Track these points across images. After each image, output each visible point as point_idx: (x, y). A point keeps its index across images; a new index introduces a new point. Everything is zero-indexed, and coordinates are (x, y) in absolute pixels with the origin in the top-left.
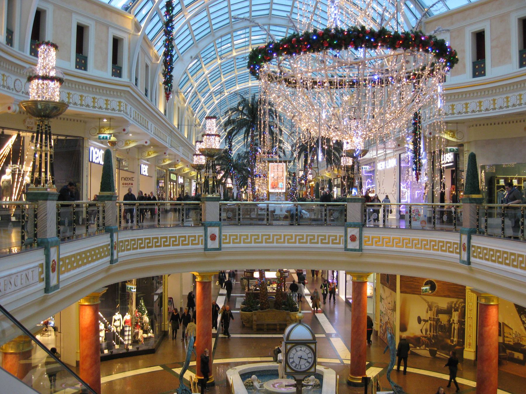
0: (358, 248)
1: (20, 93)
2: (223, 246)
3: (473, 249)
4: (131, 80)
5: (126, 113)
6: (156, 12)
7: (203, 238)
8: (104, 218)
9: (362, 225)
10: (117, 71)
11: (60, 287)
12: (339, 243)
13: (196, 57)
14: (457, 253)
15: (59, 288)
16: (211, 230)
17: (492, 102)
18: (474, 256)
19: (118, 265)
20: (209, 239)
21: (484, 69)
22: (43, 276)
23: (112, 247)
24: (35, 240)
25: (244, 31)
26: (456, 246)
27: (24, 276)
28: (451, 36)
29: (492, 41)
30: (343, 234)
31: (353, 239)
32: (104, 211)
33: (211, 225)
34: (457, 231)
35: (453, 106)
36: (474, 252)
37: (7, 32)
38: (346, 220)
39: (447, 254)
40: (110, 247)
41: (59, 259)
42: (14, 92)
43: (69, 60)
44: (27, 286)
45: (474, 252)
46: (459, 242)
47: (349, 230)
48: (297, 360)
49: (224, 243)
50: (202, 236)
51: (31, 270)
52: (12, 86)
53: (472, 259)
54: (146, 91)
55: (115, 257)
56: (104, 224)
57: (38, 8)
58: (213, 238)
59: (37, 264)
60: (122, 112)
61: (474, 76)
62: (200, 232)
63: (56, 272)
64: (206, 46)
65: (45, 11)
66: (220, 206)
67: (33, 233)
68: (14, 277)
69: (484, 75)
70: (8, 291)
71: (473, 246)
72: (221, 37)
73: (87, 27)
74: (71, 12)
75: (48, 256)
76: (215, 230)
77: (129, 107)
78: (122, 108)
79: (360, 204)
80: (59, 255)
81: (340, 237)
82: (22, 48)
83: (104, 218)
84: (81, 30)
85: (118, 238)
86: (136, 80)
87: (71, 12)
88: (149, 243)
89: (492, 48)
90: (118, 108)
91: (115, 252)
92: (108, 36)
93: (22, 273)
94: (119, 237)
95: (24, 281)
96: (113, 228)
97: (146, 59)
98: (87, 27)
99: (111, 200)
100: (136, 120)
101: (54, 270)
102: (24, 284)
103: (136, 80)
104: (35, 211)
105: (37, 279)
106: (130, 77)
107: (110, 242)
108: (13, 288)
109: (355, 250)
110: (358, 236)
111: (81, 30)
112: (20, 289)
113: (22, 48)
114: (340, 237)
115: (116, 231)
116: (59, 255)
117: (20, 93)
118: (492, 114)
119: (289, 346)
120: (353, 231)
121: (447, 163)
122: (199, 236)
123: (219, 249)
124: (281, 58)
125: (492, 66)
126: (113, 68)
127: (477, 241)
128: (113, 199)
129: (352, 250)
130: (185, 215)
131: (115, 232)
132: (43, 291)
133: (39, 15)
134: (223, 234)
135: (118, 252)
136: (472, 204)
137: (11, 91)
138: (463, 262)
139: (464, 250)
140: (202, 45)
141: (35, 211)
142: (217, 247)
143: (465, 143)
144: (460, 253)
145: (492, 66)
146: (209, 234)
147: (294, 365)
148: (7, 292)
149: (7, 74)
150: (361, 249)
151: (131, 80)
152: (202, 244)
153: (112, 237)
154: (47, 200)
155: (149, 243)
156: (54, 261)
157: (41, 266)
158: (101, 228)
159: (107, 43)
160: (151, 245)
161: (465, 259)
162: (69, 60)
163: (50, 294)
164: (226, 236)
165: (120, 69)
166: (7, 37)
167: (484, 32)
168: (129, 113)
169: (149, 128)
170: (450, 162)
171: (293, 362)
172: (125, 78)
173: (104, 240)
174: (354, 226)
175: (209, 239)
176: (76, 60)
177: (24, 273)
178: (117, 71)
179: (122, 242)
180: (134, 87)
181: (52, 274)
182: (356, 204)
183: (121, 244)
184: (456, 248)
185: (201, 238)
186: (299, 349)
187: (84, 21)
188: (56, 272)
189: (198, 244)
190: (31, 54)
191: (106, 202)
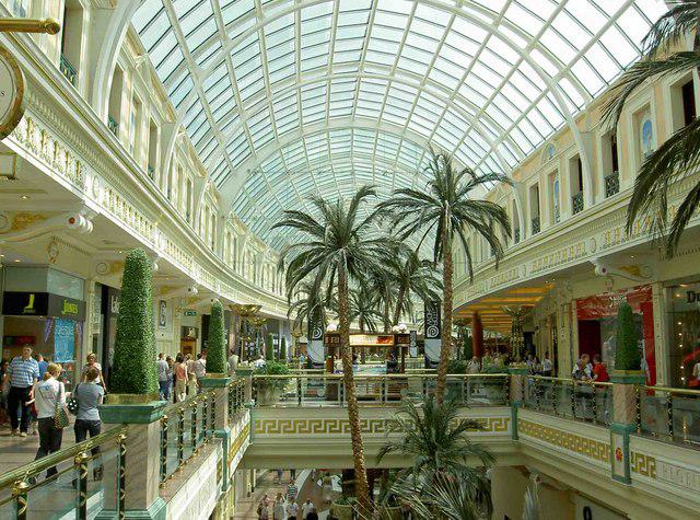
53: (633, 475)
72: (288, 145)
140: (262, 154)
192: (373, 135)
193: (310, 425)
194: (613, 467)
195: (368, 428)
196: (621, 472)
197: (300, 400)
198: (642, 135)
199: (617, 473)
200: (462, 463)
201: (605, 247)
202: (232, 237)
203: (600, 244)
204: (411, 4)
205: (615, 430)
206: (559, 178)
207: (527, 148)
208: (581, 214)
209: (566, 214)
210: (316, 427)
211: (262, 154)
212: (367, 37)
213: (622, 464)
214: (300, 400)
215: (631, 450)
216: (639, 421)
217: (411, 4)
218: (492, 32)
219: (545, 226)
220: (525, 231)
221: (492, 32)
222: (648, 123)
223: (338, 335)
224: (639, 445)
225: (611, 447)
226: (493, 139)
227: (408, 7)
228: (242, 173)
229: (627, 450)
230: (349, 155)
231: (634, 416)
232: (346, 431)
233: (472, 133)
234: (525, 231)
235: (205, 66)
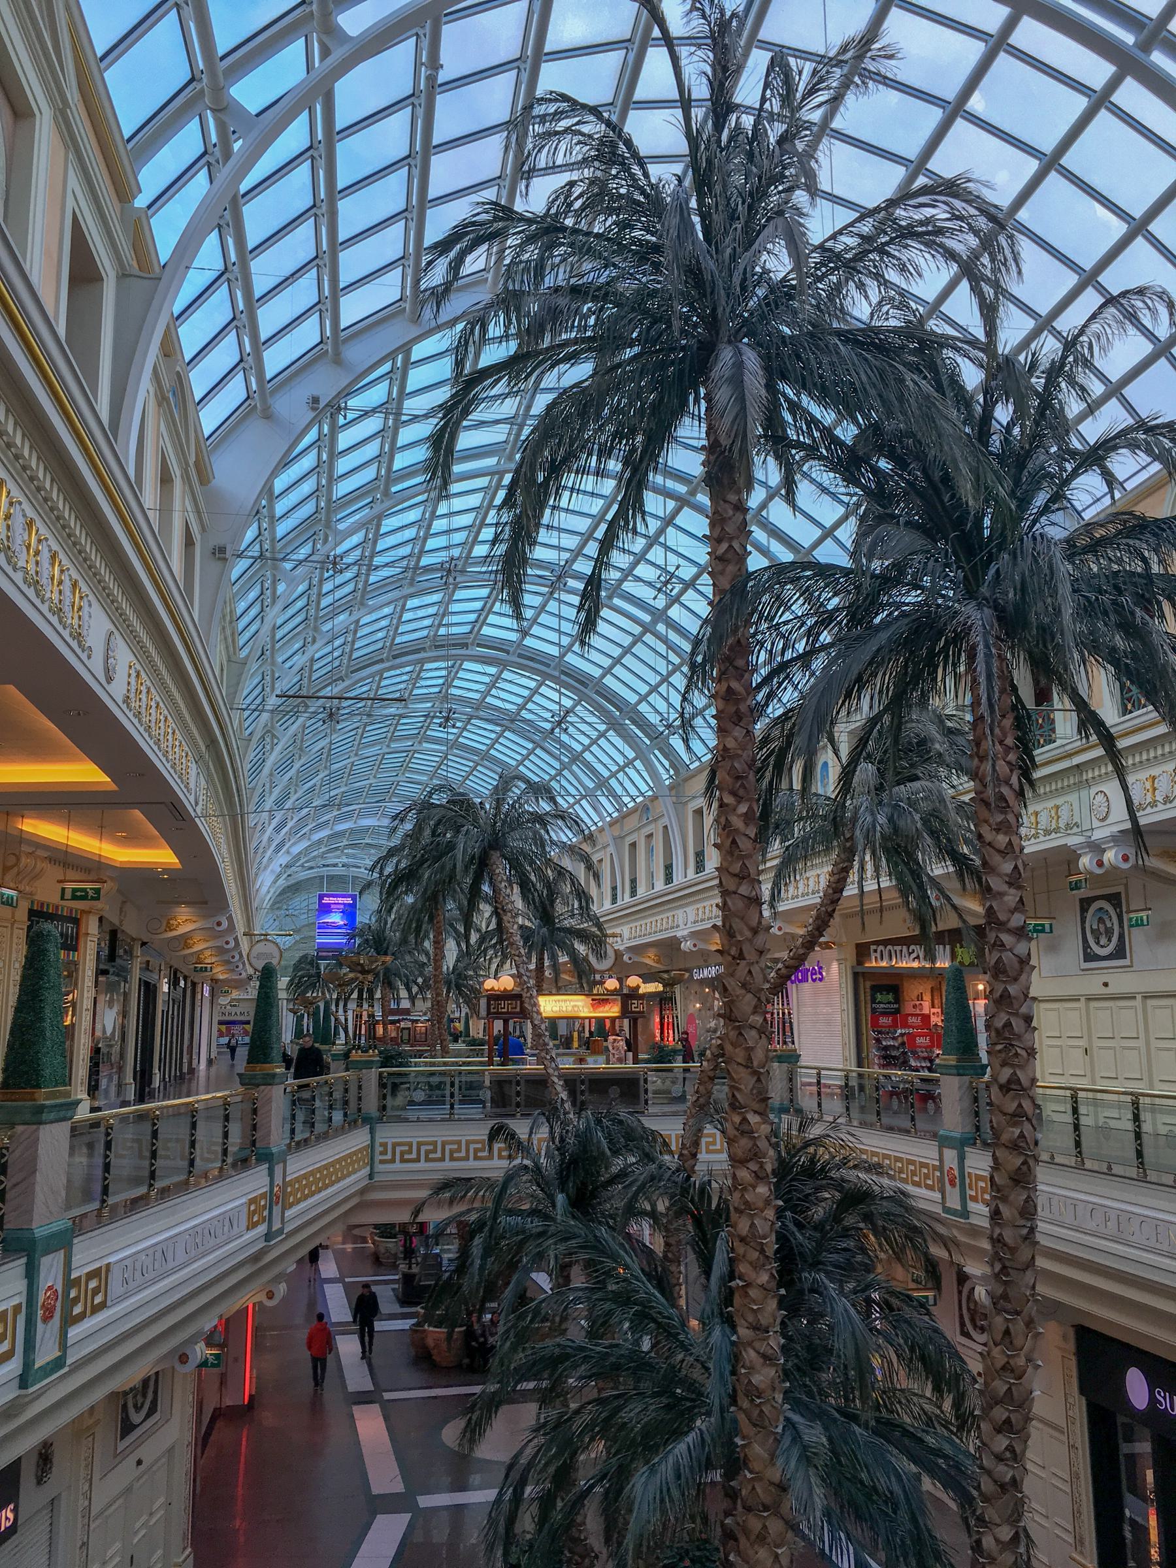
11: (69, 1362)
15: (62, 1366)
27: (159, 1255)
32: (360, 1087)
41: (69, 1283)
59: (244, 1200)
83: (360, 1099)
94: (288, 1172)
101: (46, 1319)
105: (244, 1223)
107: (21, 1299)
128: (277, 1080)
132: (16, 1382)
139: (952, 1183)
153: (31, 1273)
156: (50, 1288)
163: (31, 1390)
173: (358, 1139)
194: (943, 1197)
195: (439, 1155)
196: (954, 1203)
197: (452, 1107)
203: (691, 918)
204: (1004, 11)
205: (944, 1142)
206: (654, 842)
209: (660, 886)
210: (427, 1152)
214: (452, 1107)
215: (967, 1170)
217: (1004, 11)
218: (646, 629)
219: (641, 891)
221: (646, 629)
223: (517, 997)
225: (941, 1168)
227: (993, 17)
232: (500, 1157)
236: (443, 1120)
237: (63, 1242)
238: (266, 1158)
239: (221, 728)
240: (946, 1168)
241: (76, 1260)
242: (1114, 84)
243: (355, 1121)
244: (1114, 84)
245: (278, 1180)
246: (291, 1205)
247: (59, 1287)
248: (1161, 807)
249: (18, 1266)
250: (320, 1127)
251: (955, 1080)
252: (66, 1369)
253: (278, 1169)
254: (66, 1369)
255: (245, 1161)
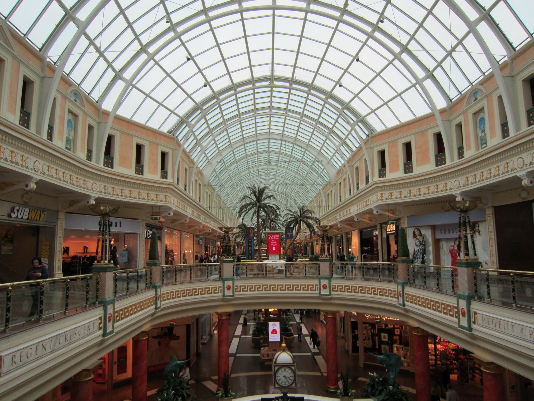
0: (328, 293)
1: (96, 192)
2: (236, 293)
3: (406, 296)
4: (174, 181)
5: (171, 203)
6: (191, 134)
7: (222, 288)
8: (151, 278)
9: (330, 278)
10: (164, 174)
11: (115, 332)
12: (315, 290)
13: (220, 162)
14: (395, 298)
15: (113, 333)
16: (227, 283)
17: (418, 190)
18: (407, 301)
19: (161, 311)
20: (226, 289)
21: (412, 168)
22: (102, 325)
23: (156, 299)
24: (97, 300)
25: (252, 144)
26: (395, 293)
27: (86, 328)
28: (389, 146)
29: (416, 149)
30: (318, 284)
31: (325, 287)
32: (151, 274)
33: (227, 279)
34: (395, 282)
35: (391, 193)
36: (407, 298)
37: (87, 151)
38: (319, 274)
39: (389, 298)
40: (154, 299)
41: (114, 312)
42: (92, 191)
43: (131, 168)
44: (88, 335)
45: (407, 298)
46: (396, 290)
47: (322, 281)
48: (283, 379)
49: (236, 291)
50: (221, 287)
51: (92, 323)
52: (90, 188)
53: (406, 303)
54: (186, 186)
55: (159, 305)
56: (151, 283)
57: (109, 134)
58: (229, 288)
59: (97, 317)
60: (168, 202)
61: (405, 173)
62: (220, 284)
63: (111, 322)
64: (227, 154)
65: (114, 136)
66: (233, 266)
67: (95, 295)
68: (78, 329)
69: (412, 172)
70: (73, 339)
71: (406, 294)
73: (144, 146)
74: (132, 136)
75: (105, 311)
76: (230, 283)
77: (172, 198)
78: (167, 200)
79: (329, 263)
80: (114, 309)
81: (316, 285)
82: (98, 162)
83: (151, 278)
84: (139, 148)
85: (161, 292)
86: (178, 179)
87: (132, 136)
88: (184, 293)
89: (416, 153)
90: (164, 200)
91: (159, 302)
92: (157, 152)
93: (84, 326)
95: (86, 331)
96: (157, 285)
97: (185, 164)
98: (144, 146)
99: (156, 266)
100: (178, 207)
101: (110, 321)
102: (86, 332)
103: (178, 179)
104: (97, 280)
105: (96, 327)
106: (173, 178)
107: (154, 295)
108: (78, 337)
109: (326, 295)
110: (328, 285)
111: (139, 148)
112: (83, 338)
113: (98, 162)
114: (316, 285)
115: (160, 287)
116: (114, 309)
117: (96, 192)
118: (418, 198)
119: (276, 368)
120: (324, 282)
121: (391, 231)
122: (219, 287)
123: (233, 296)
124: (92, 248)
125: (418, 165)
126: (161, 172)
127: (409, 290)
129: (324, 295)
130: (209, 273)
131: (159, 288)
132: (102, 336)
133: (110, 139)
134: (235, 285)
135: (161, 301)
136: (404, 264)
137: (89, 191)
138: (400, 304)
139: (400, 296)
140: (224, 154)
141: (97, 280)
142: (232, 294)
143: (402, 217)
144: (397, 298)
145: (418, 165)
146: (226, 286)
147: (280, 382)
148: (72, 340)
149: (86, 180)
150: (330, 294)
151: (174, 181)
152: (221, 293)
153: (156, 291)
154: (106, 272)
155: (184, 293)
156: (110, 314)
157: (100, 318)
158: (148, 285)
159: (157, 156)
160: (185, 295)
161: (402, 303)
162: (131, 168)
163: (106, 338)
164: (237, 286)
165: (167, 173)
166: (87, 155)
167: (411, 143)
168: (172, 203)
169: (188, 211)
170: (393, 231)
171: (280, 380)
172: (170, 180)
173: (151, 294)
174: (326, 278)
175: (226, 289)
176: (136, 168)
177: (87, 326)
178: (164, 174)
179: (164, 294)
180: (176, 186)
181: (108, 324)
182: (326, 263)
183: (164, 296)
184: (395, 294)
185: (220, 289)
186: (279, 378)
187: (141, 142)
188: (111, 322)
189: (218, 293)
190: (104, 166)
191: (153, 267)
192: (280, 142)
193: (285, 287)
195: (307, 289)
198: (478, 125)
199: (462, 324)
200: (442, 347)
201: (357, 210)
202: (208, 193)
205: (459, 297)
207: (354, 149)
208: (369, 185)
211: (214, 162)
212: (229, 137)
213: (466, 319)
215: (405, 292)
216: (409, 279)
220: (354, 190)
222: (483, 119)
224: (475, 306)
225: (458, 308)
226: (337, 144)
228: (214, 162)
229: (469, 311)
230: (269, 151)
231: (407, 278)
233: (328, 141)
234: (354, 190)
235: (193, 123)
236: (205, 281)
237: (113, 302)
238: (104, 304)
239: (163, 184)
240: (460, 308)
241: (116, 306)
242: (393, 60)
243: (150, 287)
244: (393, 60)
245: (159, 293)
246: (117, 321)
247: (112, 313)
248: (462, 188)
249: (154, 290)
250: (91, 301)
251: (465, 269)
252: (114, 334)
253: (159, 290)
254: (114, 334)
255: (94, 304)
